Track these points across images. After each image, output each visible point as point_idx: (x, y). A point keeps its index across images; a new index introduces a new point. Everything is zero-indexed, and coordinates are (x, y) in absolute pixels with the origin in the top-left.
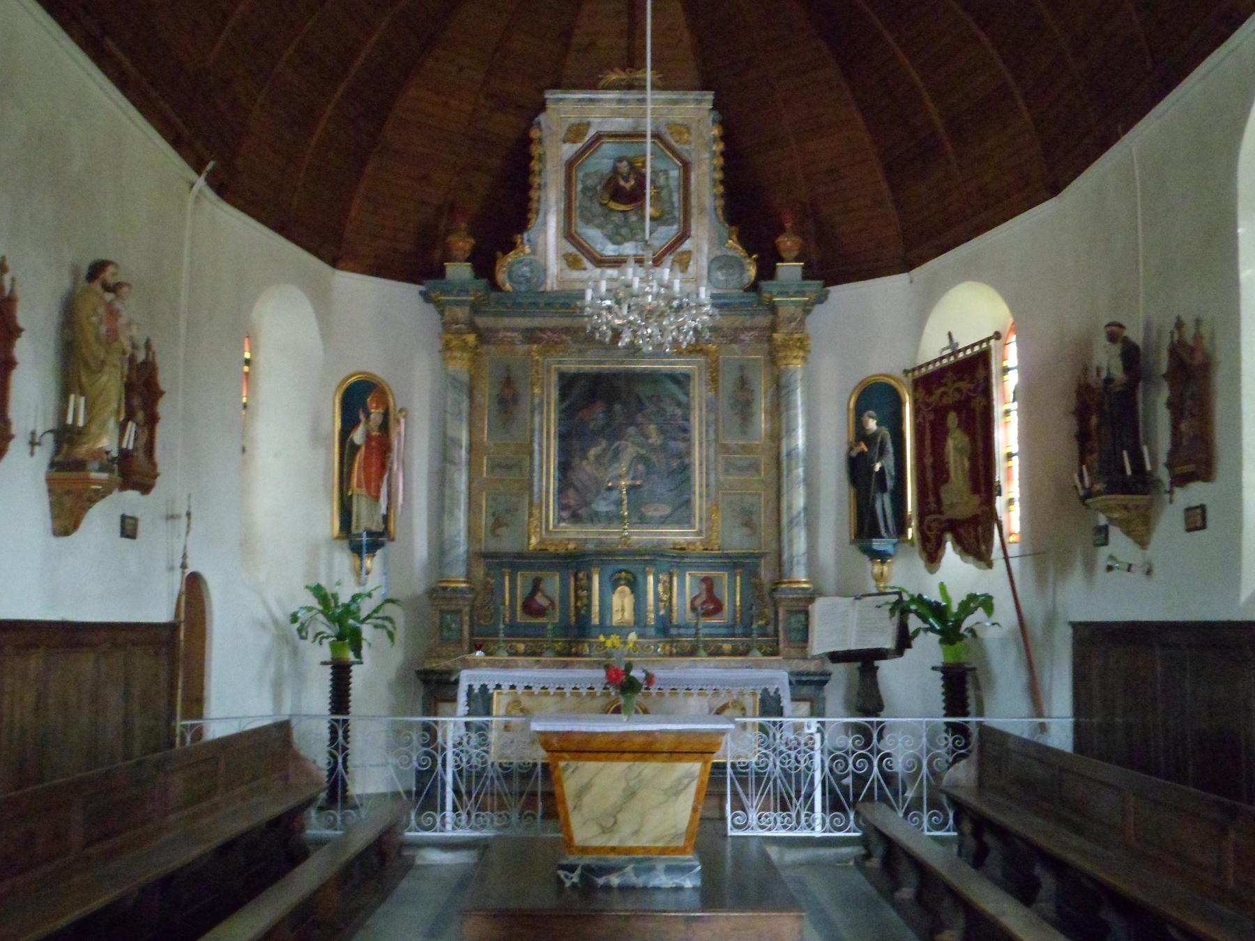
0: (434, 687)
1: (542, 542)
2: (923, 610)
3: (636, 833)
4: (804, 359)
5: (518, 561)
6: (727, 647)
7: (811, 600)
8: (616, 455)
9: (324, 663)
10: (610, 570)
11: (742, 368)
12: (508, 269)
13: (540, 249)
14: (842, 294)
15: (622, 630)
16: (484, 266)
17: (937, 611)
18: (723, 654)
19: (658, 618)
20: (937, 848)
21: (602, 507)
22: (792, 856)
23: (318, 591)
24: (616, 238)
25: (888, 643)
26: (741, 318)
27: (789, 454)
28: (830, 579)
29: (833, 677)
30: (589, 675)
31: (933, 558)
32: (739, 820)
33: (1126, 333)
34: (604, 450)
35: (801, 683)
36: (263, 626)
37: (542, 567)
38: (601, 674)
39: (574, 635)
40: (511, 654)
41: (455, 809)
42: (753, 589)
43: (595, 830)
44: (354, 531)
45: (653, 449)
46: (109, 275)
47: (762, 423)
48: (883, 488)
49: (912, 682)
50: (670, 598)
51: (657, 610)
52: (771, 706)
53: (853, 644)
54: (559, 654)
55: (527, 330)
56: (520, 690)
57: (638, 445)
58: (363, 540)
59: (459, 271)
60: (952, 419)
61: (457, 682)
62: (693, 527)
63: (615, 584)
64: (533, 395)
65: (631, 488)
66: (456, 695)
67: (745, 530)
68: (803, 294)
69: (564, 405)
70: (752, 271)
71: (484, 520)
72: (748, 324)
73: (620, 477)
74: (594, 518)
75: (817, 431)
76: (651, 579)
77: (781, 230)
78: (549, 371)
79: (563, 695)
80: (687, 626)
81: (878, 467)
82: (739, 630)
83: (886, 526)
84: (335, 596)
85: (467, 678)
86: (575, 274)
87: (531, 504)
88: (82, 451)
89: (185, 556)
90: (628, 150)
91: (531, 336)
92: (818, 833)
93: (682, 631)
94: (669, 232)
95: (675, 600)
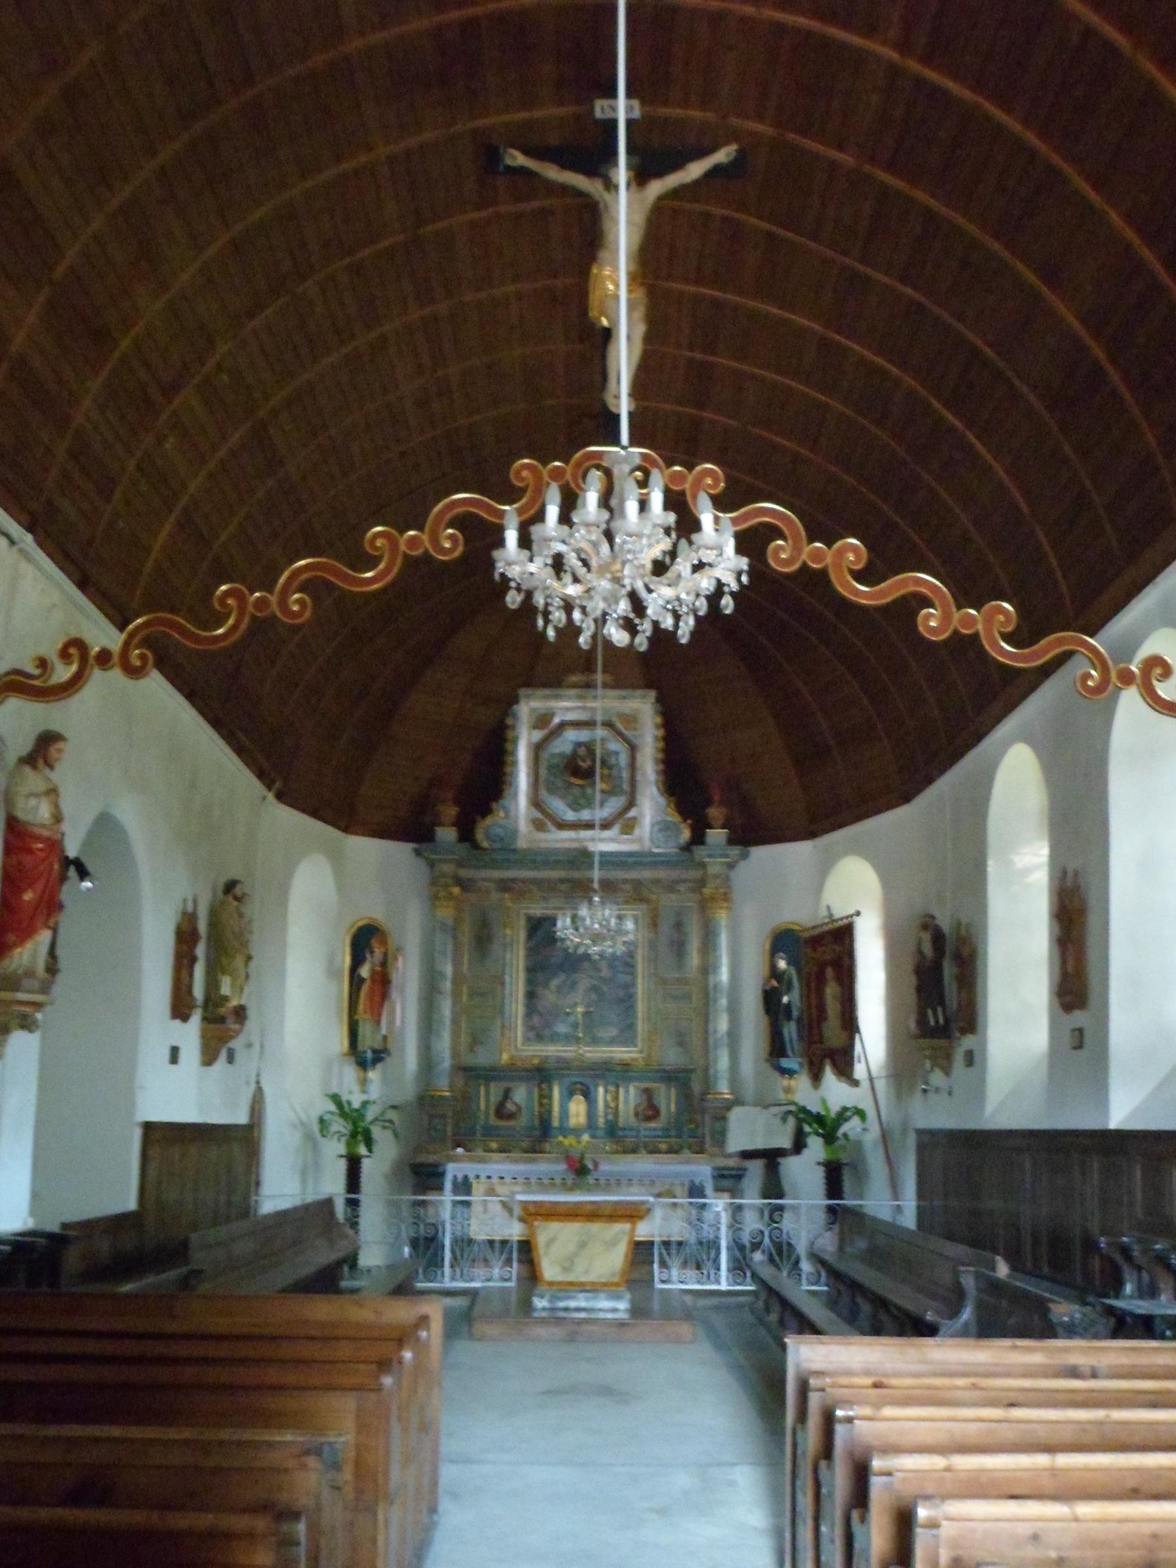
0: (423, 1176)
1: (512, 1058)
2: (810, 1119)
3: (587, 1272)
4: (729, 909)
5: (491, 1074)
6: (663, 1147)
7: (729, 1109)
8: (573, 986)
9: (342, 1156)
10: (567, 1081)
11: (678, 914)
12: (484, 829)
13: (512, 814)
14: (760, 853)
15: (577, 1132)
16: (466, 834)
17: (819, 1119)
18: (659, 1152)
19: (607, 1121)
20: (813, 1301)
21: (562, 1028)
22: (702, 1302)
23: (336, 1098)
24: (575, 806)
25: (785, 1142)
26: (678, 872)
27: (715, 987)
28: (749, 1090)
29: (748, 1174)
30: (549, 1166)
31: (816, 1077)
32: (665, 1277)
33: (937, 922)
34: (564, 981)
35: (723, 1176)
36: (295, 1126)
37: (512, 1079)
38: (562, 1167)
39: (541, 1135)
40: (485, 1151)
41: (452, 1266)
42: (686, 1095)
43: (557, 1269)
44: (360, 1048)
45: (604, 980)
46: (238, 890)
47: (694, 959)
48: (789, 1017)
49: (804, 1173)
50: (617, 1107)
51: (606, 1114)
52: (696, 1191)
53: (759, 1144)
54: (526, 1152)
55: (502, 880)
56: (495, 1180)
57: (591, 977)
58: (365, 1056)
59: (447, 834)
60: (830, 972)
61: (442, 1175)
62: (635, 1046)
63: (571, 1094)
64: (505, 935)
65: (587, 1014)
66: (443, 1184)
67: (680, 1049)
68: (726, 856)
69: (530, 944)
70: (686, 834)
71: (464, 1039)
72: (683, 876)
73: (576, 1004)
74: (554, 1038)
75: (738, 964)
76: (601, 1090)
77: (708, 802)
78: (518, 915)
79: (529, 1184)
80: (631, 1129)
81: (785, 999)
82: (673, 1133)
83: (793, 1049)
84: (349, 1103)
85: (453, 1170)
86: (542, 835)
87: (503, 1026)
88: (222, 1011)
89: (258, 1075)
90: (583, 735)
91: (505, 886)
92: (724, 1286)
93: (626, 1132)
94: (614, 805)
95: (621, 1106)
